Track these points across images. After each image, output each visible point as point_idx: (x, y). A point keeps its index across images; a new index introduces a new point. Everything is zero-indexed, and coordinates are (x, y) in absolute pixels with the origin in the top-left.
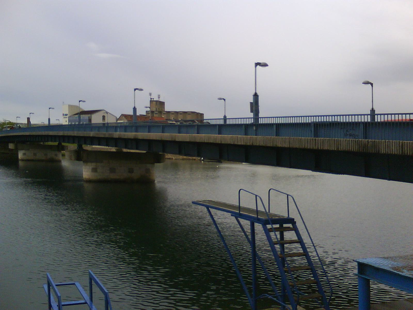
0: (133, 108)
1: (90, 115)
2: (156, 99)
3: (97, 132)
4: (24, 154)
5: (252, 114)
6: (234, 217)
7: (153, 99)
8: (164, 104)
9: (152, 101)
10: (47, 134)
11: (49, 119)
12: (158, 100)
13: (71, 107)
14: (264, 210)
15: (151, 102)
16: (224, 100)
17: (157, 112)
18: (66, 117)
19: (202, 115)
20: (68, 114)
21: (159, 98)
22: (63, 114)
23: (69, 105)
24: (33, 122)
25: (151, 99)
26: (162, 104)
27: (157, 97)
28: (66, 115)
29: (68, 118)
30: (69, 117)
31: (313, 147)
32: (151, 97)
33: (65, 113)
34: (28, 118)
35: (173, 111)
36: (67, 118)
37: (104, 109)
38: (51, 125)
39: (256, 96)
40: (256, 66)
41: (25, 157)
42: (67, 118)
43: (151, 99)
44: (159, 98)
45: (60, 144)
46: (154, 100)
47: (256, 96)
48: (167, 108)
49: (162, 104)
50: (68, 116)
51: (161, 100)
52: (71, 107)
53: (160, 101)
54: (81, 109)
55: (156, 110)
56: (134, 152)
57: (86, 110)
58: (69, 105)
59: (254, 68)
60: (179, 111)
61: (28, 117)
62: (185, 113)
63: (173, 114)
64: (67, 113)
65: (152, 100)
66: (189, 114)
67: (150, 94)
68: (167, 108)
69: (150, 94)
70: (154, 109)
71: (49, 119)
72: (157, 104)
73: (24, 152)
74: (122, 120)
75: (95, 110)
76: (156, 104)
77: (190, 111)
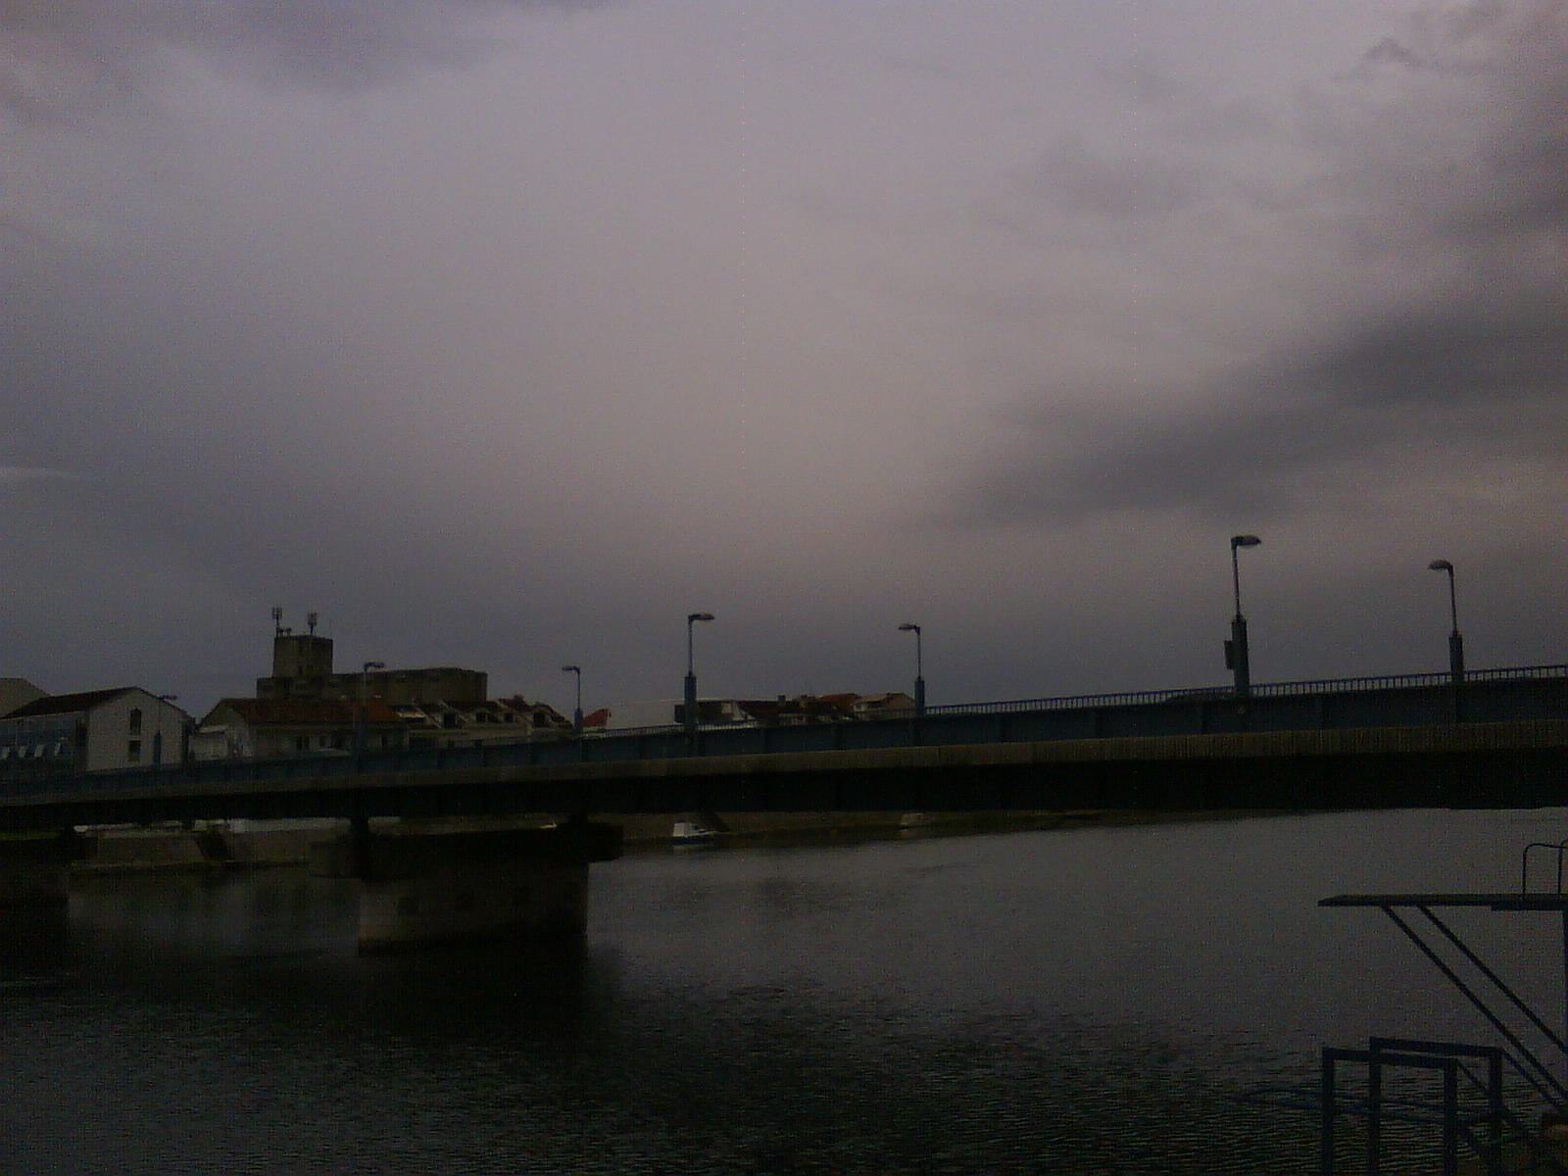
0: (686, 678)
2: (300, 629)
5: (1232, 672)
6: (1377, 908)
7: (289, 630)
9: (282, 637)
11: (1456, 642)
14: (1395, 911)
15: (282, 641)
16: (918, 629)
19: (480, 679)
21: (312, 625)
32: (278, 624)
39: (1239, 625)
40: (1234, 548)
43: (280, 631)
44: (312, 625)
47: (1239, 625)
48: (344, 661)
49: (324, 646)
51: (320, 632)
53: (315, 639)
55: (301, 672)
59: (1231, 552)
65: (285, 634)
67: (277, 615)
68: (344, 661)
69: (277, 615)
71: (1456, 642)
75: (89, 689)
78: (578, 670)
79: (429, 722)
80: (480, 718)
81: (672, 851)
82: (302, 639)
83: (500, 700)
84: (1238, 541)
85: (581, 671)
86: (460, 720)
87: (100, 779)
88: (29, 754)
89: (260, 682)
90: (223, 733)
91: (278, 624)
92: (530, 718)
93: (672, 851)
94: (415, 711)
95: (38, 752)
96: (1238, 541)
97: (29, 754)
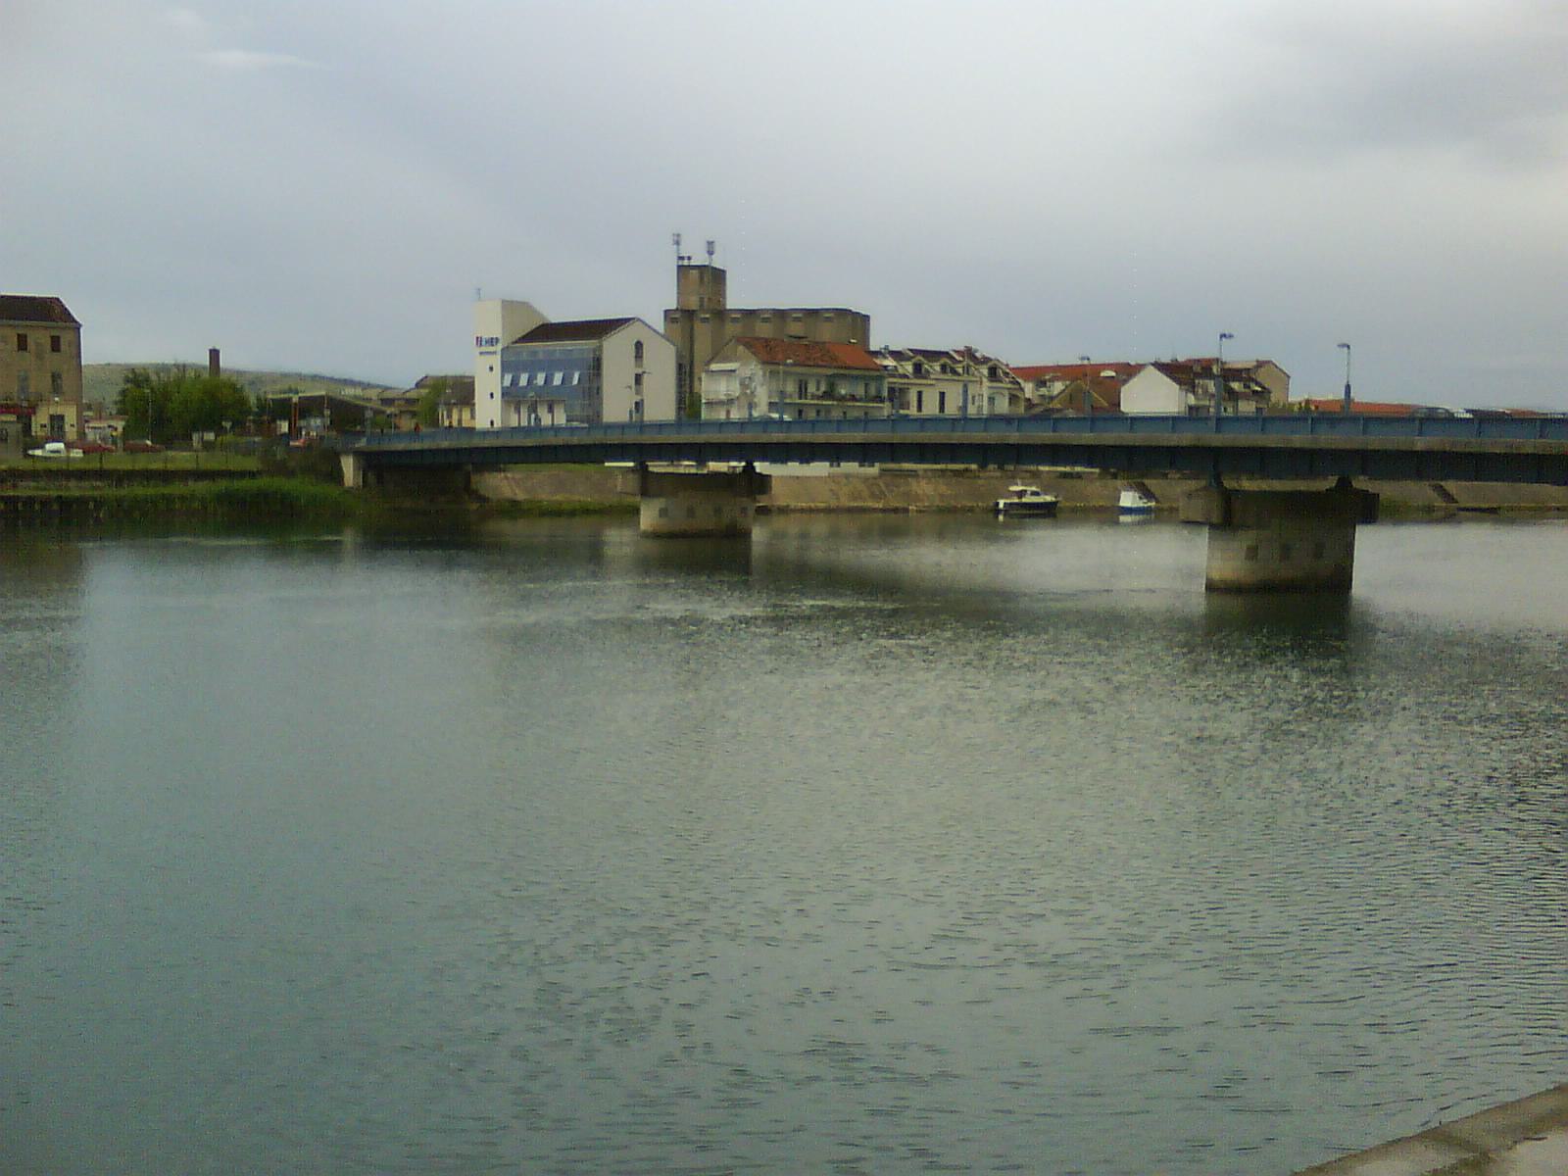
1: (592, 343)
3: (1051, 434)
4: (663, 513)
7: (689, 258)
8: (724, 279)
10: (1361, 447)
11: (1348, 388)
12: (706, 264)
13: (511, 307)
17: (707, 316)
18: (491, 349)
20: (499, 336)
21: (711, 253)
22: (479, 341)
23: (503, 301)
24: (1358, 396)
25: (681, 258)
26: (717, 277)
27: (704, 248)
28: (492, 341)
29: (499, 357)
30: (503, 350)
31: (508, 529)
32: (678, 250)
33: (486, 336)
34: (211, 351)
35: (768, 310)
36: (495, 353)
37: (642, 318)
38: (223, 376)
41: (665, 525)
42: (495, 353)
44: (711, 253)
45: (1344, 483)
46: (693, 263)
48: (737, 298)
50: (499, 347)
52: (511, 307)
54: (543, 318)
55: (701, 305)
56: (1473, 539)
57: (555, 318)
58: (503, 301)
60: (819, 307)
61: (211, 347)
62: (812, 313)
63: (765, 320)
64: (497, 332)
65: (686, 262)
66: (828, 319)
70: (693, 303)
71: (1348, 388)
72: (705, 279)
73: (663, 506)
74: (730, 361)
76: (701, 278)
77: (737, 308)
78: (1348, 347)
79: (901, 371)
80: (944, 367)
81: (1117, 523)
82: (702, 268)
83: (956, 351)
84: (1223, 336)
85: (1351, 347)
86: (928, 371)
87: (610, 426)
88: (548, 380)
89: (666, 311)
90: (734, 371)
91: (678, 250)
92: (985, 372)
93: (1117, 523)
94: (886, 358)
95: (523, 380)
96: (1223, 336)
97: (548, 380)
